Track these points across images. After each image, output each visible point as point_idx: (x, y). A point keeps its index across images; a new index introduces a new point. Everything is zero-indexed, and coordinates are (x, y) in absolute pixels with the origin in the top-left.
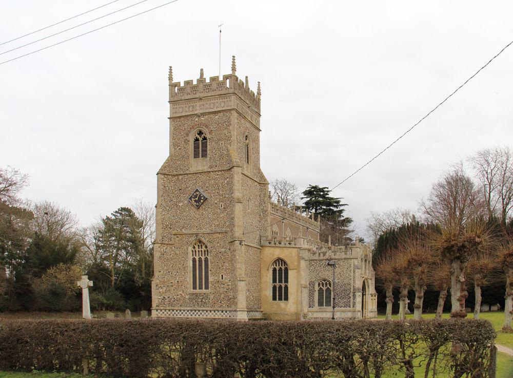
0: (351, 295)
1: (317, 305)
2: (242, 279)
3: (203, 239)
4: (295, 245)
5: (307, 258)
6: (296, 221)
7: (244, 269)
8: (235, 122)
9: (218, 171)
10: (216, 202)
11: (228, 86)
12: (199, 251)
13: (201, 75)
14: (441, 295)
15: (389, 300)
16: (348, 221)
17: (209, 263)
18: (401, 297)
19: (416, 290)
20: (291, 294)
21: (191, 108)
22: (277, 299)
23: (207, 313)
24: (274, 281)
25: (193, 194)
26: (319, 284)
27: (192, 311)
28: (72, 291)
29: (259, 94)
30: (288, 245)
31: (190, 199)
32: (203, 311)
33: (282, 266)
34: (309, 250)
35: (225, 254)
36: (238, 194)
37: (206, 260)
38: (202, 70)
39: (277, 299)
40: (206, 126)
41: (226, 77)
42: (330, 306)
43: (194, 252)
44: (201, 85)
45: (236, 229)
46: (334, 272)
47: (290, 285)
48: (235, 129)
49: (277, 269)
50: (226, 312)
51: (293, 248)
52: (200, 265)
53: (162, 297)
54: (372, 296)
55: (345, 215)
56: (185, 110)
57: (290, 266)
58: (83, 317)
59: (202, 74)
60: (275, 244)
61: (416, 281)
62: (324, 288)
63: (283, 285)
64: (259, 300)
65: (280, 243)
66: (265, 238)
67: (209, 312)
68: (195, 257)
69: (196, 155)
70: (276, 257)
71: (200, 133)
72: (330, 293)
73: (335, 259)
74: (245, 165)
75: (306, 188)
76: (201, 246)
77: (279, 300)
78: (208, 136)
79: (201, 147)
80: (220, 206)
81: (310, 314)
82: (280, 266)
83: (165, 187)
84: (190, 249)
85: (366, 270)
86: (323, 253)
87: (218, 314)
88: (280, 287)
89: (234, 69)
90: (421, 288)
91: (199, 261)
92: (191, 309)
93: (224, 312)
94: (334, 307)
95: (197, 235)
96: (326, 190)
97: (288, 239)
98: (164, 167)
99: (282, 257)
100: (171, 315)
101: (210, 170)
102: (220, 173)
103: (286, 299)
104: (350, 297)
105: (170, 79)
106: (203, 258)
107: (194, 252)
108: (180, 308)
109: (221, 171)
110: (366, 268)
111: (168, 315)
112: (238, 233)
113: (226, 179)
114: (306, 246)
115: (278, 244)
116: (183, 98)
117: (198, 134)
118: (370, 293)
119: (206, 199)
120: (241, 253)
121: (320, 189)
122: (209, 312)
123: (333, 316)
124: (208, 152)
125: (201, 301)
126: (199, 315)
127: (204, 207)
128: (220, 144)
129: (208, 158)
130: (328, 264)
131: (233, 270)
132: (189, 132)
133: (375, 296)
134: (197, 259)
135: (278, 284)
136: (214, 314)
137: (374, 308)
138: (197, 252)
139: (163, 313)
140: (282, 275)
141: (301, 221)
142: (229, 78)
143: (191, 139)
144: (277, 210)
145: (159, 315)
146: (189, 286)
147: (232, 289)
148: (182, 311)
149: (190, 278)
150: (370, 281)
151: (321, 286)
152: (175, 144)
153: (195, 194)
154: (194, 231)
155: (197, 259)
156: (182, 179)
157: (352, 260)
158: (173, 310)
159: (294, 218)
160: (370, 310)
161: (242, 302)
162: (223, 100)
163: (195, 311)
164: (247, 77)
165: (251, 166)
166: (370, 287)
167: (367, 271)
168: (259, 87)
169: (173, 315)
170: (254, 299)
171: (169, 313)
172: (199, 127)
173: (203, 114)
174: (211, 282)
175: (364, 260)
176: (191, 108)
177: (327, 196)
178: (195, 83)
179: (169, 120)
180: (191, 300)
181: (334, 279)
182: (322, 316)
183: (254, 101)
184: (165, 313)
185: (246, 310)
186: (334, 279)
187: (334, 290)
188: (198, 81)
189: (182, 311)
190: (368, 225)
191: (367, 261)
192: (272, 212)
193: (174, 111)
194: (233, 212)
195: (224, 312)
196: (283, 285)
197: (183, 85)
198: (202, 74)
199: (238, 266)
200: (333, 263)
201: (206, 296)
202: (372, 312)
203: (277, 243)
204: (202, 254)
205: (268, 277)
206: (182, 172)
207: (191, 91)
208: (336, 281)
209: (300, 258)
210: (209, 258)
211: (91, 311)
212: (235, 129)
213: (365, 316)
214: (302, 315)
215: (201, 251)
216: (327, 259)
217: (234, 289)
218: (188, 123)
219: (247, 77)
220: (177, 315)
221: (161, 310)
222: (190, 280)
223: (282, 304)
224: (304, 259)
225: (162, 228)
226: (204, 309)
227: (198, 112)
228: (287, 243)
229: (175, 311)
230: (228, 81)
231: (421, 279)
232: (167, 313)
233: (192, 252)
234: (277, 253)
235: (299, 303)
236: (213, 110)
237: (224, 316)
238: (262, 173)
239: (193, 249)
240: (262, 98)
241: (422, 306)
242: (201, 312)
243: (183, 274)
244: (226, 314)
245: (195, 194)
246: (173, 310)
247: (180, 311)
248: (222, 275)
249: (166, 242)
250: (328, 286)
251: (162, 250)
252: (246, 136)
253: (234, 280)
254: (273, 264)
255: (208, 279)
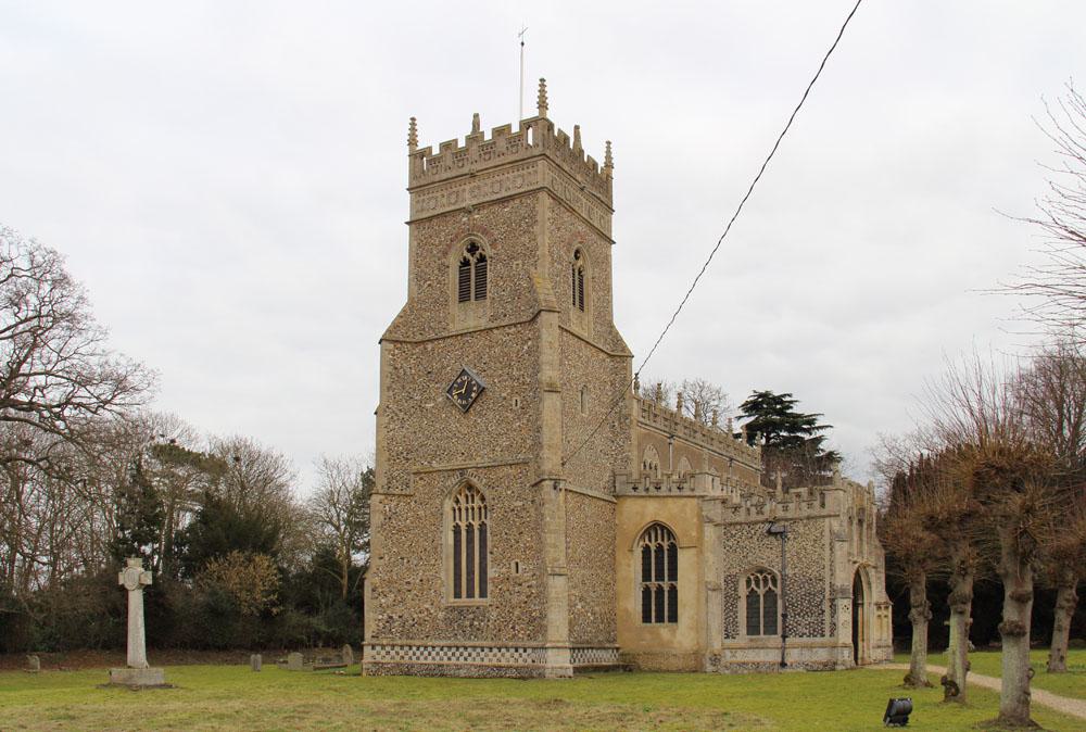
0: (826, 606)
1: (745, 631)
2: (557, 570)
3: (475, 481)
4: (693, 490)
5: (718, 520)
6: (701, 443)
7: (563, 547)
8: (547, 217)
9: (509, 326)
10: (504, 395)
11: (530, 142)
12: (467, 509)
13: (474, 126)
14: (1061, 601)
15: (920, 614)
16: (831, 457)
17: (488, 535)
18: (955, 603)
19: (1006, 575)
20: (685, 606)
21: (454, 196)
22: (762, 631)
23: (482, 654)
24: (646, 576)
25: (455, 382)
26: (748, 582)
27: (450, 648)
28: (249, 607)
29: (609, 165)
30: (675, 492)
31: (449, 391)
32: (474, 647)
33: (663, 540)
34: (724, 502)
35: (524, 514)
36: (550, 373)
37: (483, 526)
38: (476, 116)
39: (762, 631)
40: (485, 232)
41: (526, 125)
42: (775, 633)
43: (456, 511)
44: (475, 147)
45: (545, 453)
46: (783, 551)
47: (681, 584)
48: (547, 232)
49: (653, 548)
50: (525, 651)
51: (689, 497)
52: (470, 541)
53: (385, 616)
54: (879, 608)
55: (825, 446)
56: (442, 203)
57: (682, 541)
58: (129, 664)
59: (476, 124)
60: (647, 490)
61: (1005, 541)
62: (761, 591)
63: (666, 585)
64: (610, 620)
65: (658, 488)
66: (624, 478)
67: (486, 650)
68: (460, 523)
69: (464, 297)
70: (648, 520)
71: (473, 248)
72: (776, 602)
73: (786, 520)
74: (574, 312)
75: (746, 396)
76: (473, 496)
77: (657, 622)
78: (489, 252)
79: (473, 278)
80: (514, 403)
81: (728, 653)
82: (659, 541)
83: (396, 368)
84: (449, 504)
85: (861, 544)
86: (756, 506)
87: (508, 655)
88: (660, 590)
89: (543, 105)
90: (1023, 564)
91: (467, 531)
92: (449, 642)
93: (521, 651)
94: (784, 637)
95: (462, 471)
96: (788, 399)
97: (675, 477)
98: (395, 326)
99: (662, 519)
100: (407, 658)
101: (493, 325)
102: (513, 329)
103: (674, 618)
104: (823, 611)
105: (412, 142)
106: (476, 524)
107: (457, 511)
108: (425, 642)
109: (515, 325)
110: (861, 540)
111: (398, 659)
112: (550, 461)
113: (526, 342)
114: (717, 493)
115: (653, 491)
116: (437, 178)
117: (469, 251)
118: (875, 599)
119: (482, 391)
120: (555, 506)
121: (774, 398)
122: (486, 650)
123: (783, 658)
124: (489, 286)
125: (471, 625)
126: (466, 659)
127: (478, 408)
128: (514, 266)
129: (488, 301)
130: (770, 533)
131: (539, 550)
132: (449, 246)
133: (887, 608)
134: (476, 527)
135: (653, 584)
136: (499, 655)
137: (885, 636)
138: (463, 512)
139: (388, 653)
140: (650, 558)
141: (715, 442)
142: (532, 124)
143: (454, 262)
144: (655, 416)
145: (379, 658)
146: (443, 590)
147: (538, 596)
148: (430, 649)
149: (447, 570)
150: (872, 572)
151: (753, 586)
152: (418, 275)
153: (459, 381)
154: (458, 462)
155: (476, 527)
156: (433, 350)
157: (827, 520)
158: (410, 647)
159: (699, 435)
160: (873, 642)
161: (558, 624)
162: (521, 172)
163: (458, 648)
164: (577, 128)
165: (589, 316)
166: (874, 588)
167: (865, 547)
168: (608, 152)
169: (410, 658)
170: (595, 619)
171: (402, 653)
172: (470, 235)
173: (478, 207)
174: (491, 579)
175: (855, 521)
176: (454, 196)
177: (789, 411)
178: (462, 144)
179: (408, 227)
180: (449, 622)
181: (784, 567)
182: (757, 659)
183: (596, 183)
184: (393, 653)
185: (567, 644)
186: (784, 567)
187: (784, 594)
188: (468, 139)
189: (430, 649)
190: (874, 461)
191: (865, 526)
192: (642, 420)
193: (419, 207)
194: (539, 413)
195: (521, 651)
196: (666, 585)
197: (999, 681)
198: (476, 124)
199: (550, 539)
200: (782, 530)
201: (480, 613)
202: (879, 647)
203: (652, 488)
204: (473, 515)
205: (632, 569)
206: (433, 336)
207: (454, 162)
208: (789, 572)
209: (704, 520)
210: (488, 522)
211: (147, 646)
212: (547, 232)
213: (863, 658)
214: (708, 655)
215: (473, 509)
216: (767, 521)
217: (541, 595)
218: (448, 228)
219: (577, 128)
220: (418, 658)
221: (383, 647)
222: (447, 575)
223: (664, 630)
224: (711, 521)
225: (389, 460)
226: (477, 643)
227: (468, 202)
228: (674, 486)
229: (414, 649)
230: (530, 131)
231: (1025, 531)
232: (495, 655)
233: (452, 512)
234: (652, 511)
235: (701, 627)
236: (499, 196)
237: (520, 660)
238: (618, 333)
239: (455, 505)
240: (614, 173)
241: (1028, 629)
242: (469, 650)
243: (433, 562)
244: (524, 655)
245: (459, 381)
246: (410, 647)
247: (426, 647)
248: (517, 564)
249: (397, 491)
250: (770, 585)
251: (387, 508)
252: (577, 252)
253: (541, 573)
254: (642, 537)
255: (486, 573)
